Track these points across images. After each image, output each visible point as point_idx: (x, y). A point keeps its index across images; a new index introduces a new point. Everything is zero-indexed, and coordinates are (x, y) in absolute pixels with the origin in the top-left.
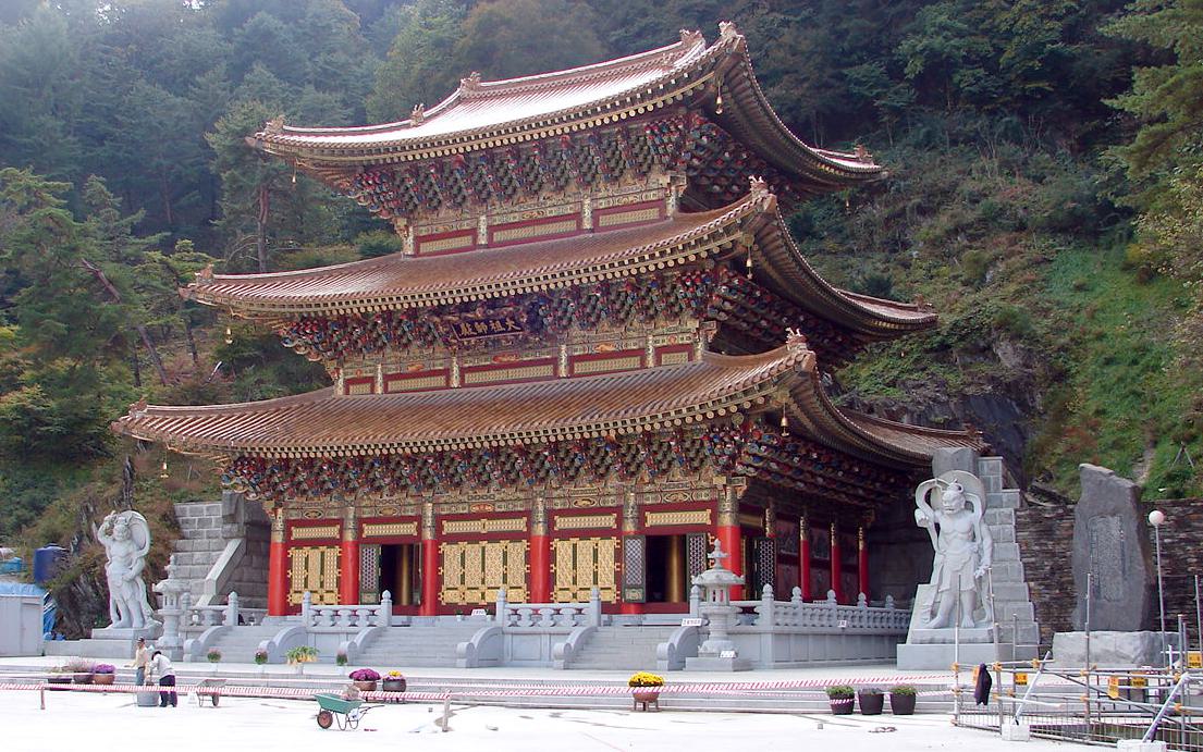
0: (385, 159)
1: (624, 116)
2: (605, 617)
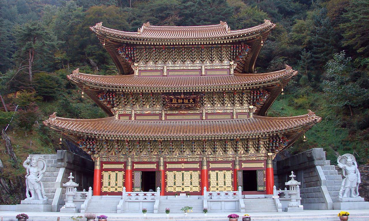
0: (137, 43)
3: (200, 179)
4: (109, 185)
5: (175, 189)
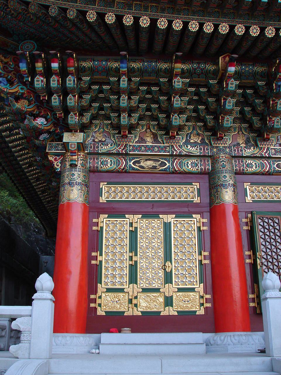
3: (204, 253)
4: (133, 279)
5: (135, 301)
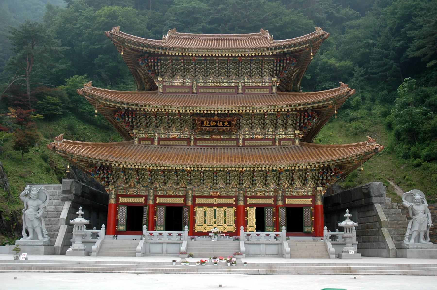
1: (173, 54)
2: (287, 237)
